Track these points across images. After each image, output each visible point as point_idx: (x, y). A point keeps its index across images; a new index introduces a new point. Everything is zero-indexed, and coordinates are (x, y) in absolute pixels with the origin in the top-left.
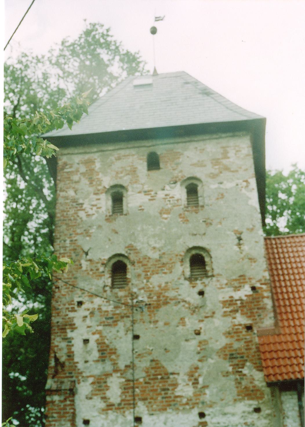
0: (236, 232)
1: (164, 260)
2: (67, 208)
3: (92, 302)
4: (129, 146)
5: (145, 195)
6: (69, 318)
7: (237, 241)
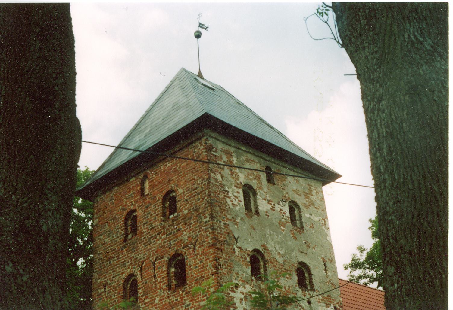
0: (323, 258)
1: (286, 267)
2: (217, 191)
3: (245, 288)
4: (257, 154)
5: (268, 203)
6: (230, 297)
7: (324, 267)
